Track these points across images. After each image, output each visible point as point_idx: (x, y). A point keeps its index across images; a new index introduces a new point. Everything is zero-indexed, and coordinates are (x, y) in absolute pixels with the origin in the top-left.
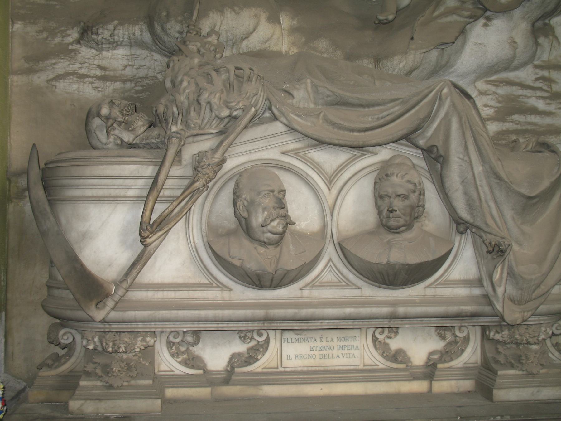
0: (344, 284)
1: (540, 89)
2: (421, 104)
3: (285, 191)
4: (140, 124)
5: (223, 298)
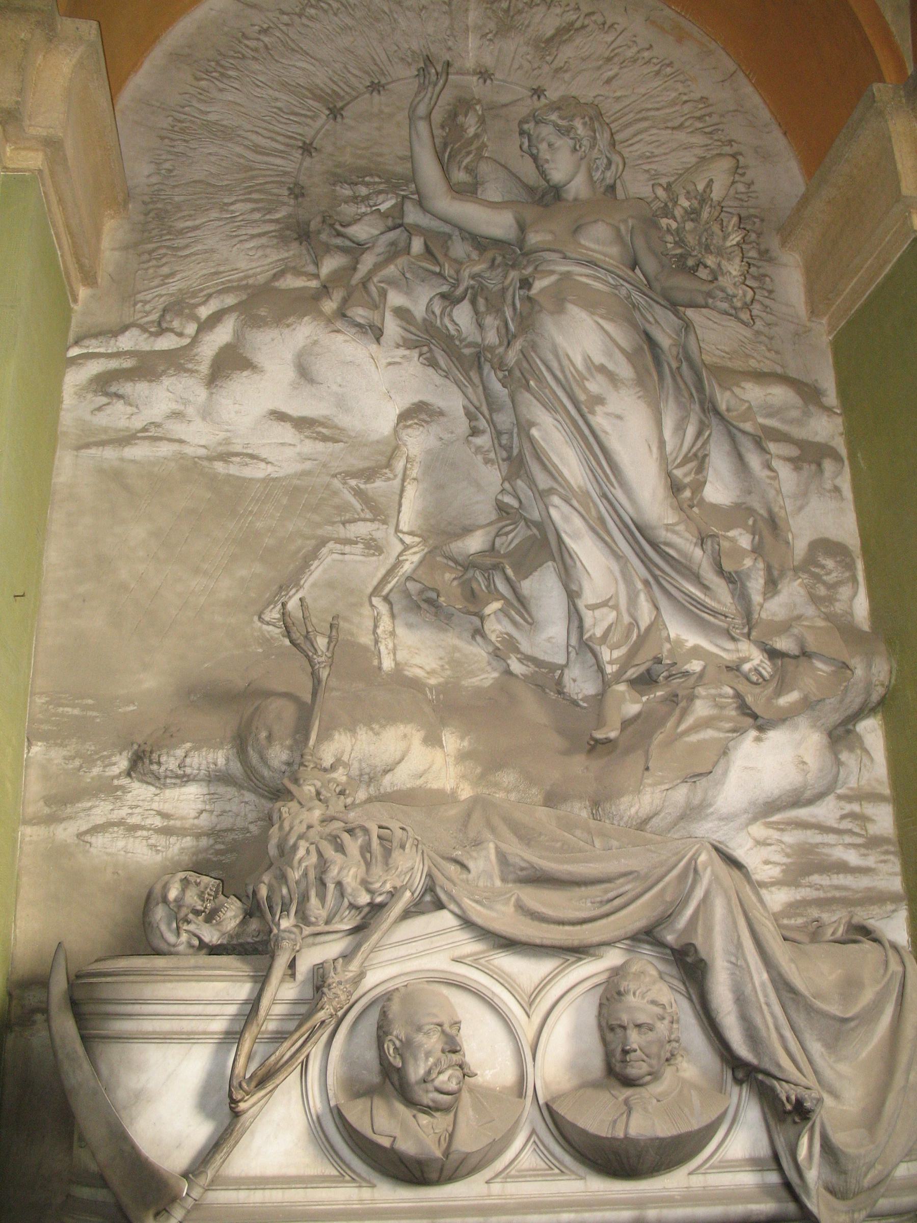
0: (556, 1171)
1: (850, 832)
2: (667, 879)
3: (460, 1022)
4: (232, 914)
5: (361, 1201)
